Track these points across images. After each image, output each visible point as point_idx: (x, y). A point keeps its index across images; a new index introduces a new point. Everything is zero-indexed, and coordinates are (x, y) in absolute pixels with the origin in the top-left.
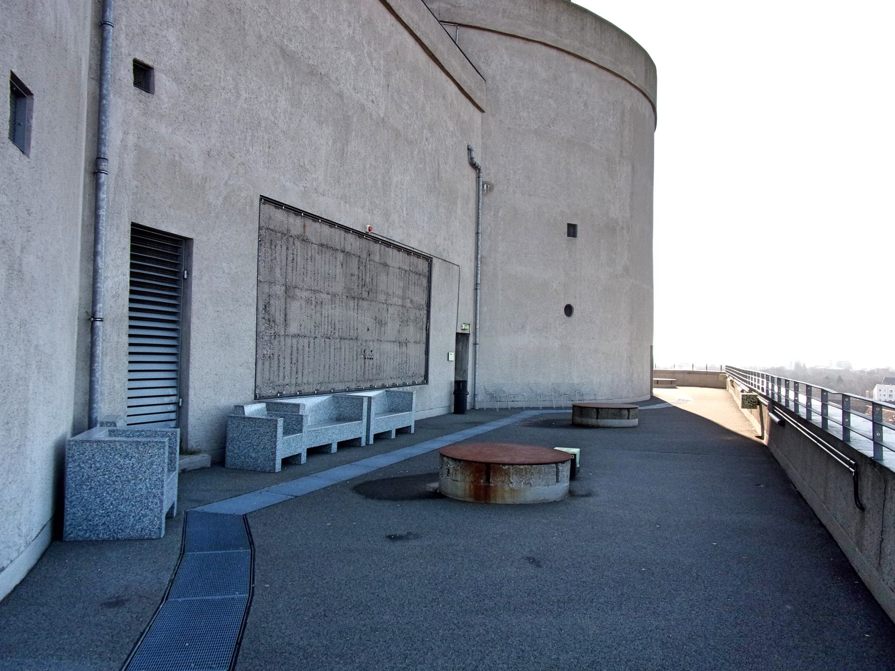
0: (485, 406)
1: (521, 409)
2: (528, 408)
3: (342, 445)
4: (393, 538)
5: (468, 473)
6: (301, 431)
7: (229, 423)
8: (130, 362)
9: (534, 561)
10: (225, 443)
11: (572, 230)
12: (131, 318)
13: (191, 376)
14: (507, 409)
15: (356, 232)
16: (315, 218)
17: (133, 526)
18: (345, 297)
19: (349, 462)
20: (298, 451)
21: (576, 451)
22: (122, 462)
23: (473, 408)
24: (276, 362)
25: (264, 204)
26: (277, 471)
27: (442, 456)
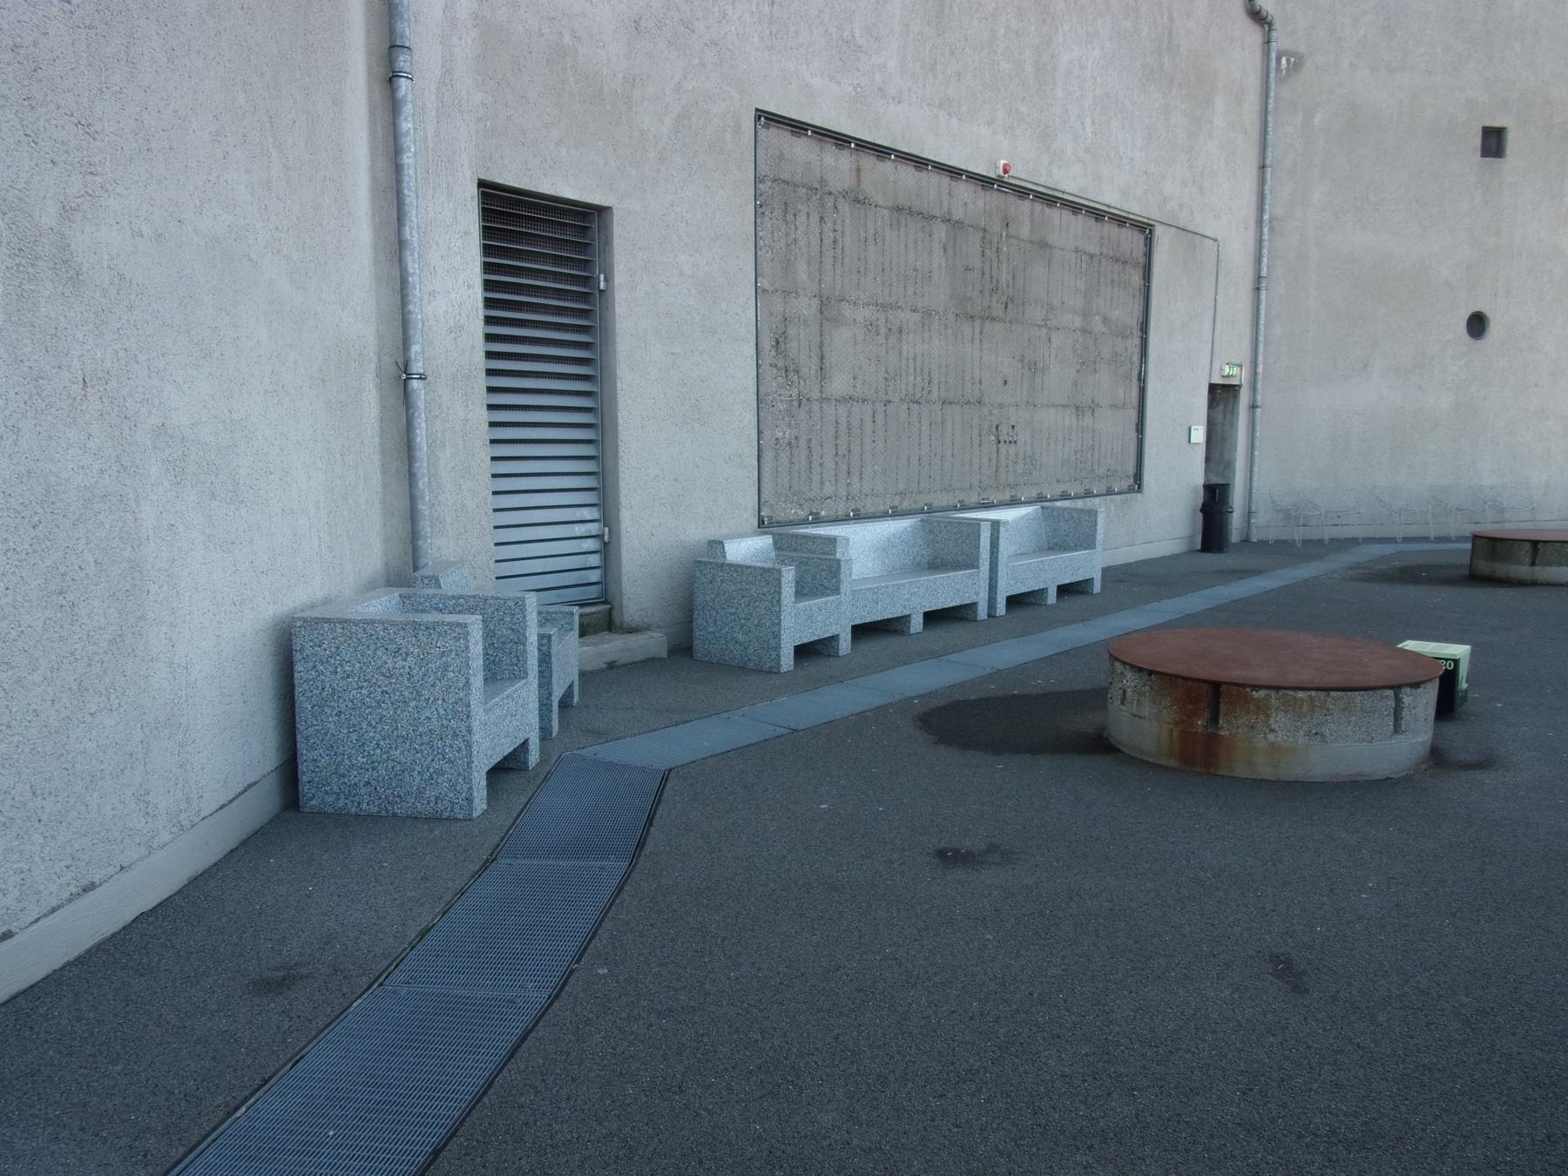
0: (1271, 535)
1: (1354, 541)
2: (1369, 540)
3: (932, 618)
4: (948, 857)
5: (1167, 702)
6: (837, 591)
7: (701, 574)
8: (494, 459)
9: (1288, 972)
10: (691, 611)
11: (1493, 142)
12: (490, 372)
13: (622, 484)
14: (1320, 542)
15: (974, 177)
16: (882, 152)
17: (420, 792)
18: (952, 317)
19: (935, 655)
20: (973, 599)
21: (1460, 651)
22: (390, 665)
23: (1246, 541)
24: (804, 453)
25: (766, 126)
26: (784, 669)
27: (1114, 658)
